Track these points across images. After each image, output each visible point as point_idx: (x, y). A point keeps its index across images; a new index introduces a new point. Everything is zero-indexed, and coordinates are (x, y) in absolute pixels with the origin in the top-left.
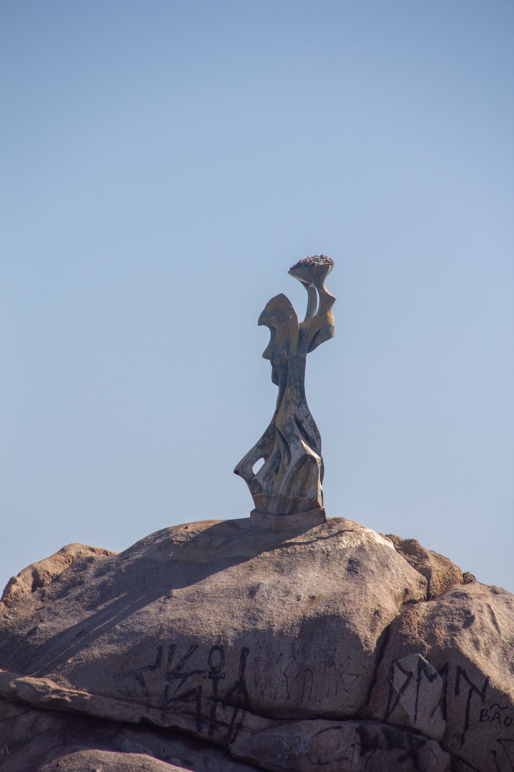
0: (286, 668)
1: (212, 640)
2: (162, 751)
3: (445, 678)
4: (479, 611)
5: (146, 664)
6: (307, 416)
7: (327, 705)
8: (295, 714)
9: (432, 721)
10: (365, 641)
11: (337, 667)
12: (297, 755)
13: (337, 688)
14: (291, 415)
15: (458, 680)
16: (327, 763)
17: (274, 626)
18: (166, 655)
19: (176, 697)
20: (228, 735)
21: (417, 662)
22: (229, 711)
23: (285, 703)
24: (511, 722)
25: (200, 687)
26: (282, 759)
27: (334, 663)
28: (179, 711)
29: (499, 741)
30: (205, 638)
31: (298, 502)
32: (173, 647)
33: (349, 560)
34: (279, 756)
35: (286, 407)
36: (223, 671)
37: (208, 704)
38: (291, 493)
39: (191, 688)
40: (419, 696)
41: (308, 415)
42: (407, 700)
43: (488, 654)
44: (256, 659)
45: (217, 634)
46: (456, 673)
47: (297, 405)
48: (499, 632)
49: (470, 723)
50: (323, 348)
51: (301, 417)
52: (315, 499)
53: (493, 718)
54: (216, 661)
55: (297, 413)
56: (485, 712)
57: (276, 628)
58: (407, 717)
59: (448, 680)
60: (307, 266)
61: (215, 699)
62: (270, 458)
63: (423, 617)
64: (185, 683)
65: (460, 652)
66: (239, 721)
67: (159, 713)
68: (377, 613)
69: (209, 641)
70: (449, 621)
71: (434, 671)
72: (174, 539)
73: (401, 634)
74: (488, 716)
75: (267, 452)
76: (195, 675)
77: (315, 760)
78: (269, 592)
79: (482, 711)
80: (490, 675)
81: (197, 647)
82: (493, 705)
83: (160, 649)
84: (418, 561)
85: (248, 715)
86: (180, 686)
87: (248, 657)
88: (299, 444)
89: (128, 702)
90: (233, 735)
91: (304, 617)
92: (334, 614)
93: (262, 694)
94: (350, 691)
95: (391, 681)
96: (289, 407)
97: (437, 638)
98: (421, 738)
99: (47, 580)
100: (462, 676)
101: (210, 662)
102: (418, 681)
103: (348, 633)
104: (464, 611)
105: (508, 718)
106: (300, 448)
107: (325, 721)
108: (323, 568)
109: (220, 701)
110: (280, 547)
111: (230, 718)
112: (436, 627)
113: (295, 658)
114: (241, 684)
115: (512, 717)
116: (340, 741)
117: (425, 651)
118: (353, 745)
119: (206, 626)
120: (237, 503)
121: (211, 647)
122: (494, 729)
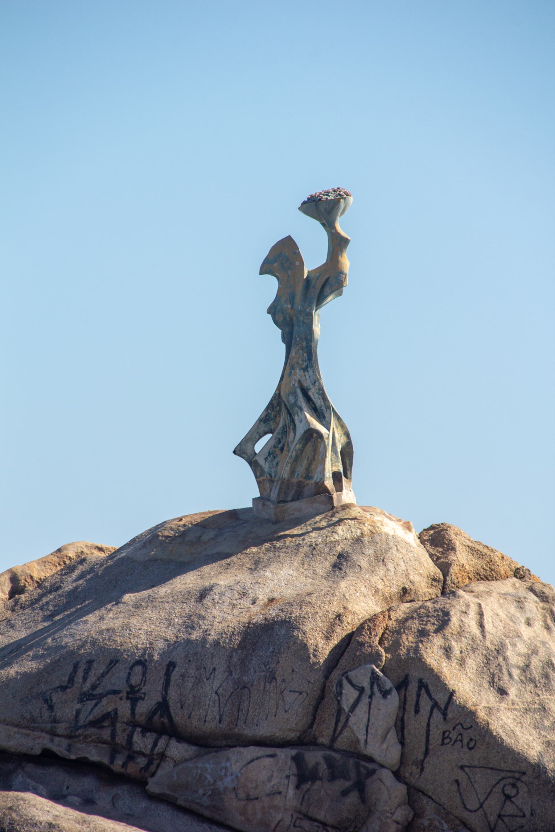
0: (219, 685)
1: (135, 653)
2: (65, 788)
3: (403, 694)
4: (463, 612)
5: (57, 684)
6: (315, 383)
7: (264, 730)
8: (206, 744)
9: (385, 746)
10: (315, 650)
11: (279, 683)
12: (221, 789)
13: (277, 708)
14: (295, 381)
15: (418, 696)
16: (257, 798)
17: (209, 635)
18: (80, 673)
19: (87, 722)
20: (146, 768)
21: (369, 675)
22: (150, 738)
23: (216, 727)
24: (475, 744)
25: (116, 711)
26: (204, 794)
27: (275, 678)
28: (90, 740)
29: (462, 767)
30: (128, 651)
31: (304, 486)
32: (90, 662)
33: (339, 554)
34: (201, 792)
35: (291, 372)
36: (143, 691)
37: (125, 730)
38: (296, 475)
39: (105, 712)
40: (371, 715)
41: (317, 381)
42: (358, 720)
43: (462, 663)
44: (183, 676)
45: (144, 646)
46: (415, 687)
47: (303, 369)
48: (484, 637)
49: (431, 747)
50: (332, 304)
51: (307, 383)
52: (321, 481)
53: (456, 741)
54: (135, 680)
55: (303, 380)
56: (448, 733)
57: (213, 637)
58: (358, 741)
59: (407, 696)
60: (314, 201)
61: (134, 724)
62: (275, 433)
63: (397, 621)
64: (99, 705)
65: (422, 661)
66: (161, 750)
67: (65, 742)
68: (339, 616)
69: (132, 655)
70: (422, 624)
71: (388, 684)
72: (160, 534)
73: (358, 641)
74: (450, 738)
75: (272, 427)
76: (109, 696)
77: (242, 795)
78: (222, 594)
79: (444, 732)
80: (456, 688)
81: (117, 661)
82: (457, 725)
83: (76, 666)
84: (443, 553)
85: (173, 742)
86: (93, 709)
87: (174, 673)
88: (303, 417)
89: (30, 729)
90: (153, 768)
91: (249, 623)
92: (285, 619)
93: (189, 717)
94: (290, 711)
95: (339, 698)
96: (293, 371)
97: (400, 645)
98: (371, 766)
99: (29, 585)
100: (423, 691)
101: (128, 679)
102: (370, 697)
103: (295, 642)
104: (443, 612)
105: (471, 740)
106: (304, 422)
107: (257, 748)
108: (303, 564)
109: (139, 726)
110: (271, 540)
111: (149, 747)
112: (404, 632)
113: (231, 673)
114: (163, 706)
115: (477, 739)
116: (273, 772)
117: (381, 661)
118: (288, 777)
119: (134, 637)
120: (240, 490)
121: (133, 662)
122: (456, 753)
